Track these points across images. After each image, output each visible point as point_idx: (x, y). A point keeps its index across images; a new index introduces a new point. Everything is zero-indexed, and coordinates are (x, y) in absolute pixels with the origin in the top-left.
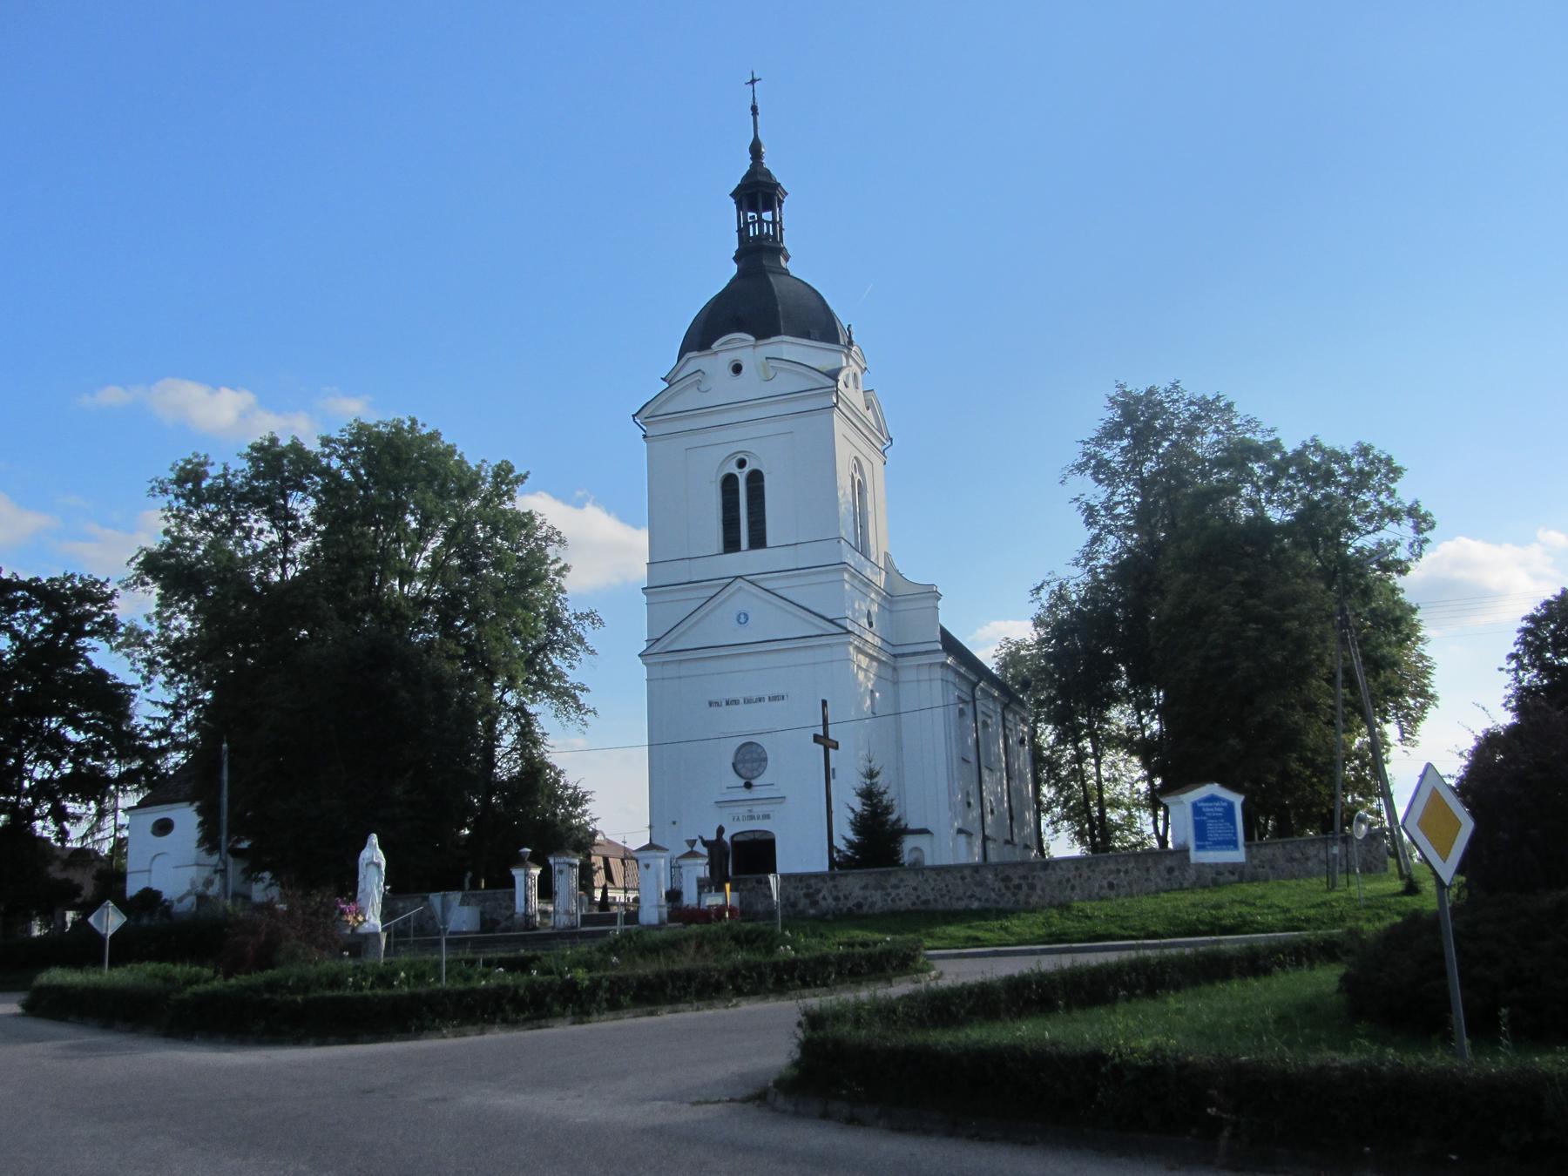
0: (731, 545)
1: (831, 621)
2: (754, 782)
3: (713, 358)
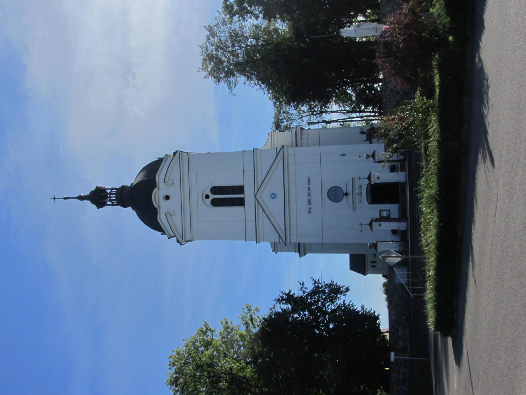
0: (241, 202)
1: (277, 155)
2: (345, 192)
3: (161, 208)
